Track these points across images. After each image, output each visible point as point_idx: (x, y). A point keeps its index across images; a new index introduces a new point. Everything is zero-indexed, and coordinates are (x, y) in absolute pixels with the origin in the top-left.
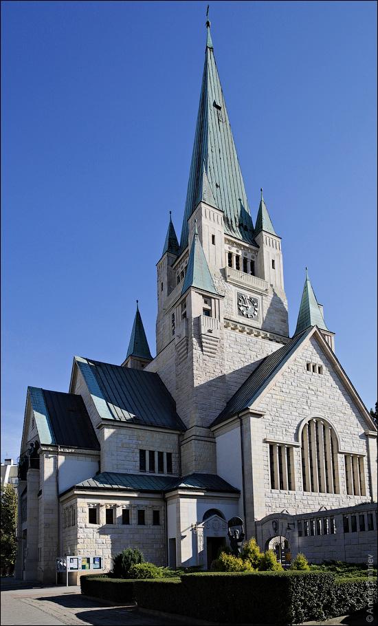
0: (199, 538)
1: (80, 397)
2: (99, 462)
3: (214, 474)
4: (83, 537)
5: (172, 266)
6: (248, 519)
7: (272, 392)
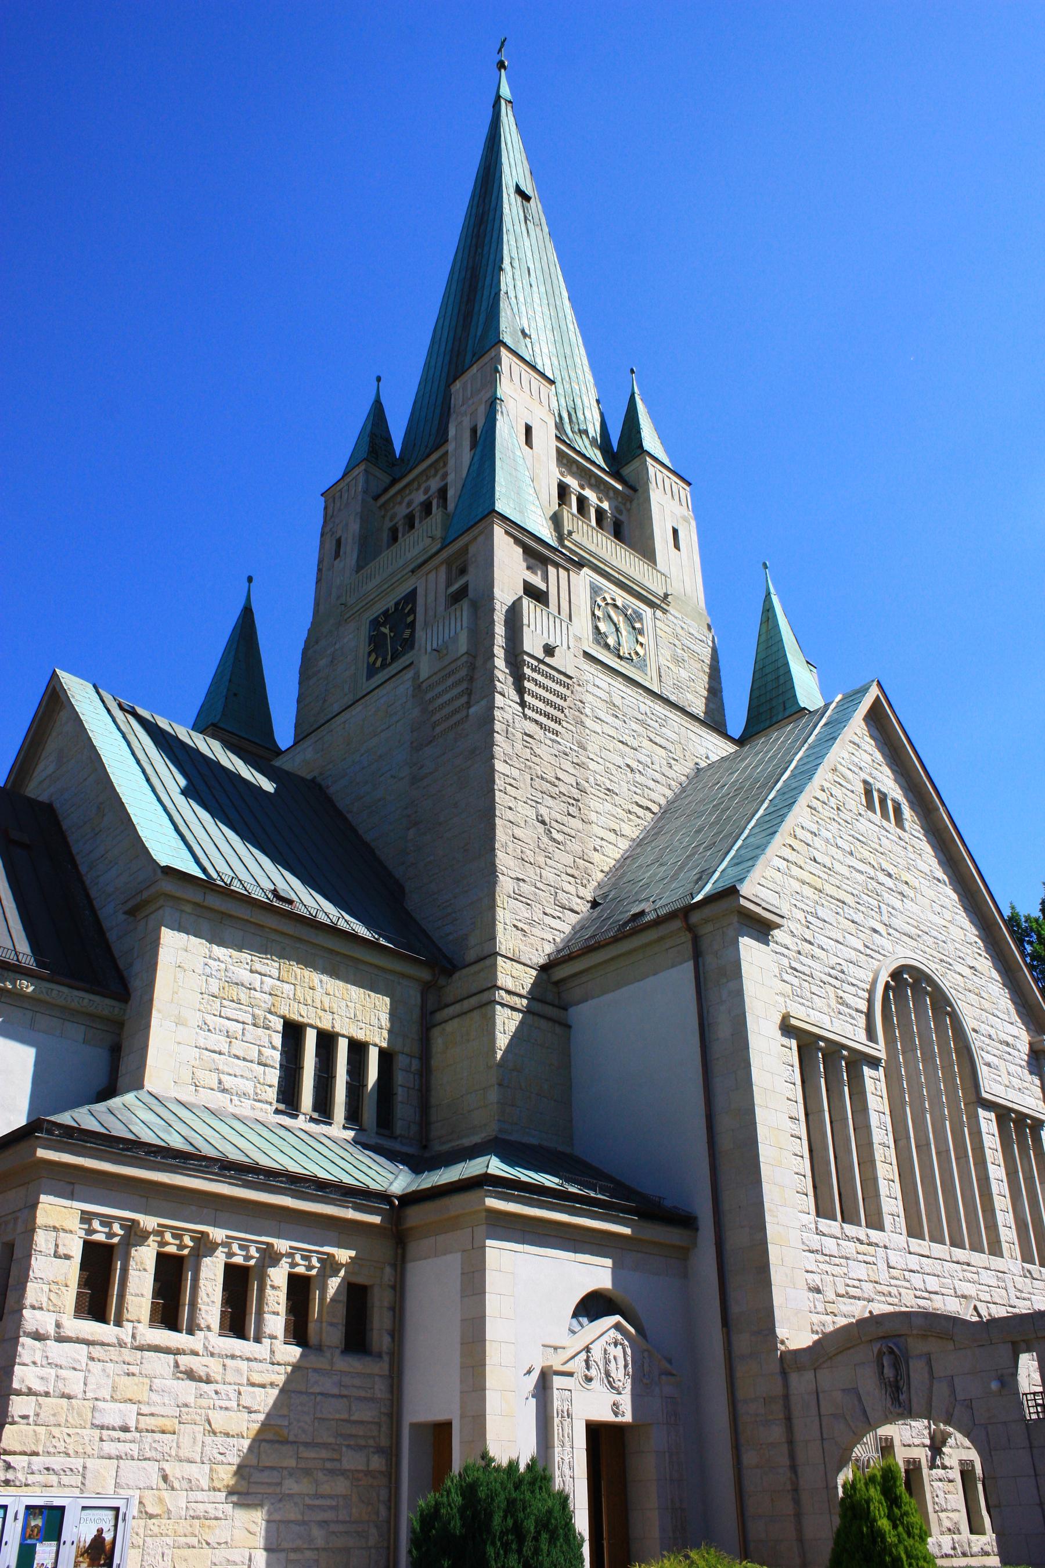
0: (556, 1421)
1: (48, 809)
3: (560, 1149)
4: (38, 1386)
5: (376, 498)
6: (743, 1342)
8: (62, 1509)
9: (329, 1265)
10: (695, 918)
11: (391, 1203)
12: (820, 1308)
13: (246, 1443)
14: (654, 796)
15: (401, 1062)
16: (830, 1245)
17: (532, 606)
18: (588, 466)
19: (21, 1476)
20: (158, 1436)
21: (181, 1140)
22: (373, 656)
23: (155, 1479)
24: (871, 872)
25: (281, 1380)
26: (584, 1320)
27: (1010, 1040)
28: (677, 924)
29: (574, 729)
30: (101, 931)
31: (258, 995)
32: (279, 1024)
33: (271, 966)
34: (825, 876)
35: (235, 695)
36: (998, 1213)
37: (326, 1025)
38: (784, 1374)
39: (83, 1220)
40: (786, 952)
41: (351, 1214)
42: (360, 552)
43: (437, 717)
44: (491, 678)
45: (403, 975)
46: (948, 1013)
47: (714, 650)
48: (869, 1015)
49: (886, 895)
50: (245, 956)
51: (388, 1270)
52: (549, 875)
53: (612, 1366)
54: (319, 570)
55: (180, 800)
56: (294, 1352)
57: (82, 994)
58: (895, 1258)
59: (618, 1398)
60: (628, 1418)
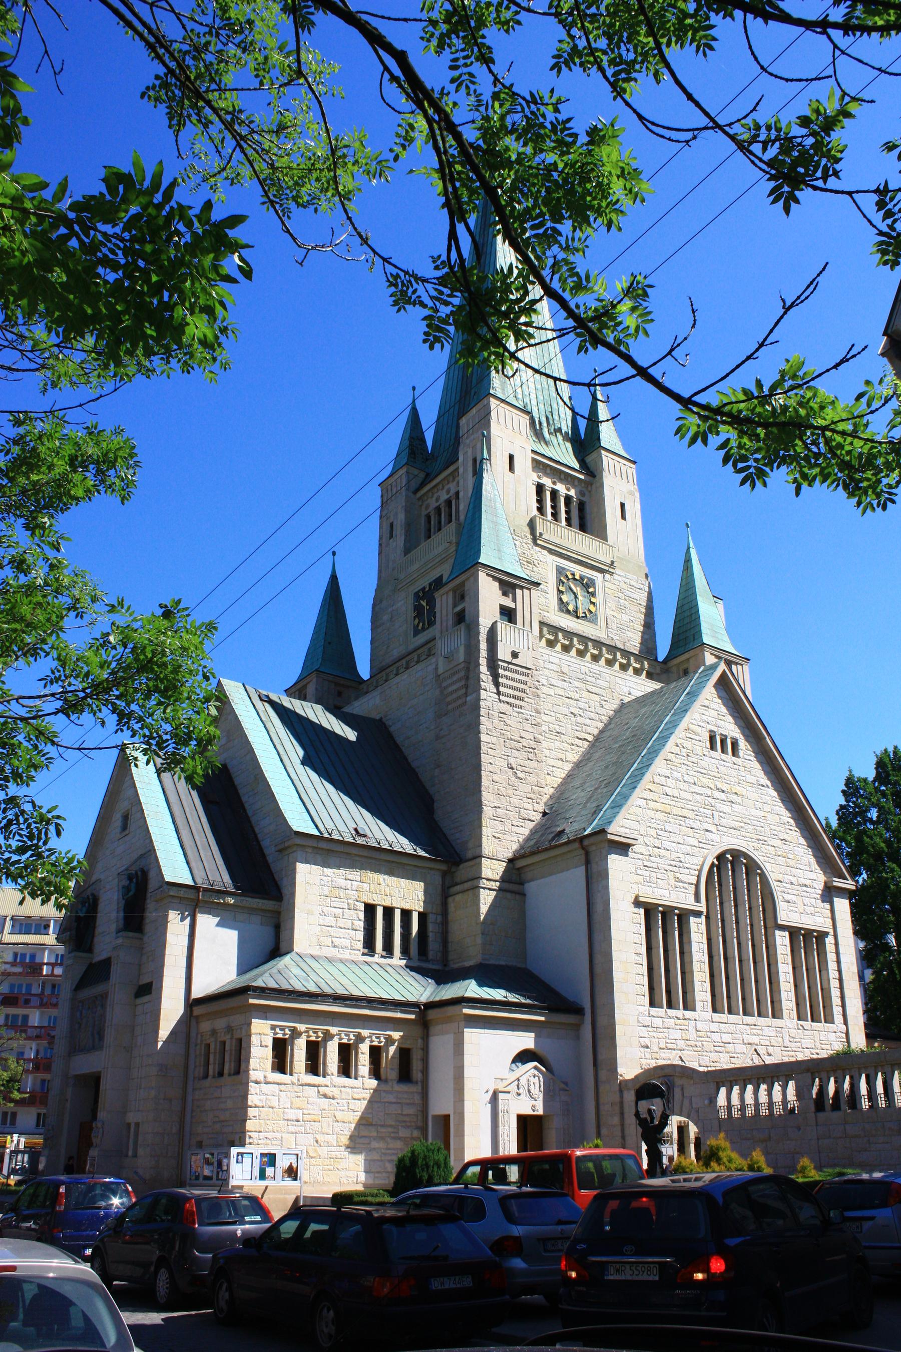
0: (500, 1114)
2: (277, 928)
3: (519, 965)
4: (260, 1104)
5: (416, 492)
6: (603, 1074)
7: (647, 794)
8: (274, 1155)
9: (390, 1041)
10: (586, 842)
11: (420, 1008)
12: (648, 1055)
13: (353, 1126)
14: (589, 730)
15: (431, 918)
16: (658, 1022)
17: (504, 626)
18: (558, 467)
19: (256, 1141)
20: (312, 1123)
21: (314, 985)
22: (417, 621)
23: (313, 1142)
24: (709, 792)
25: (368, 1096)
26: (519, 1064)
27: (808, 882)
28: (576, 845)
29: (532, 701)
30: (263, 855)
31: (349, 892)
32: (362, 907)
33: (355, 875)
34: (674, 803)
35: (330, 643)
36: (782, 993)
37: (388, 904)
38: (621, 1091)
39: (272, 1029)
40: (640, 856)
41: (399, 1015)
42: (406, 536)
43: (449, 699)
44: (478, 680)
45: (431, 869)
46: (759, 874)
47: (650, 593)
48: (697, 886)
49: (718, 805)
50: (342, 871)
51: (420, 1041)
52: (515, 801)
53: (532, 1088)
54: (380, 545)
55: (300, 768)
56: (374, 1083)
57: (257, 900)
58: (700, 1026)
59: (535, 1103)
60: (540, 1112)
